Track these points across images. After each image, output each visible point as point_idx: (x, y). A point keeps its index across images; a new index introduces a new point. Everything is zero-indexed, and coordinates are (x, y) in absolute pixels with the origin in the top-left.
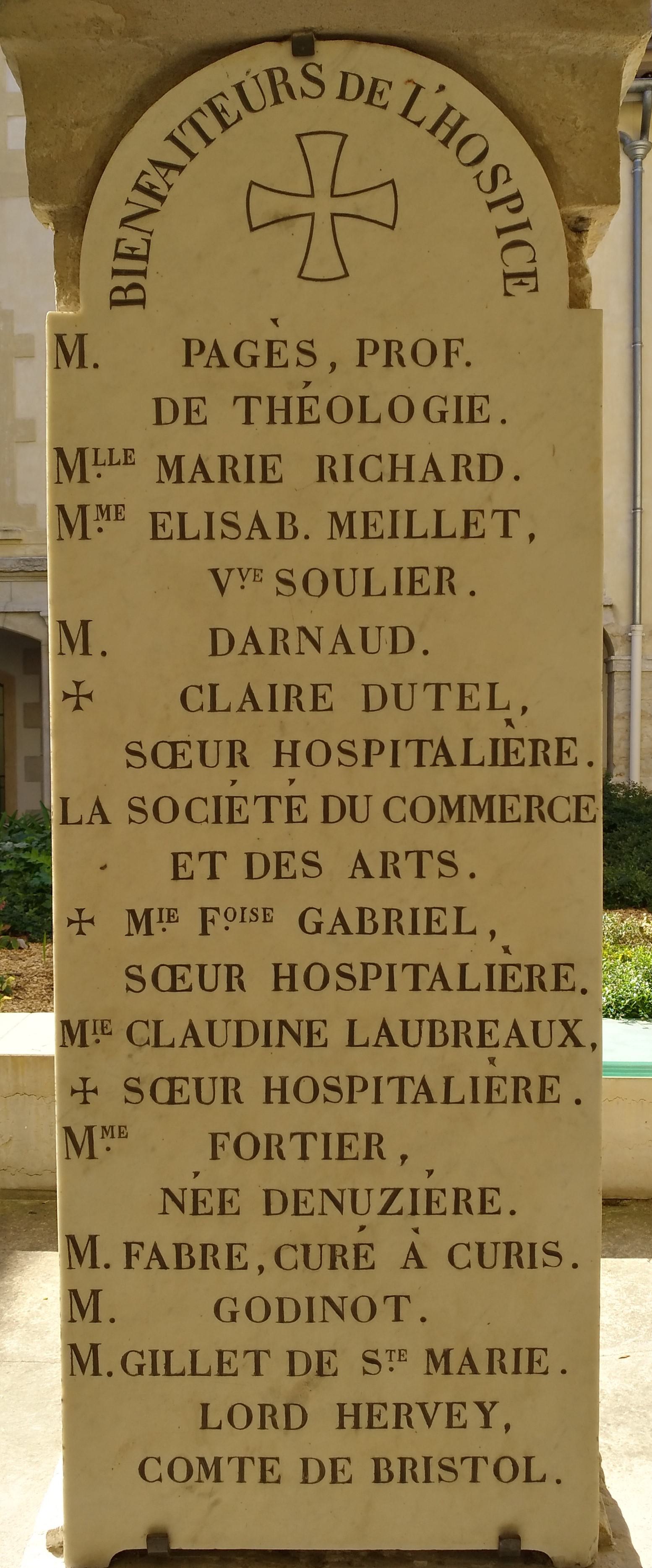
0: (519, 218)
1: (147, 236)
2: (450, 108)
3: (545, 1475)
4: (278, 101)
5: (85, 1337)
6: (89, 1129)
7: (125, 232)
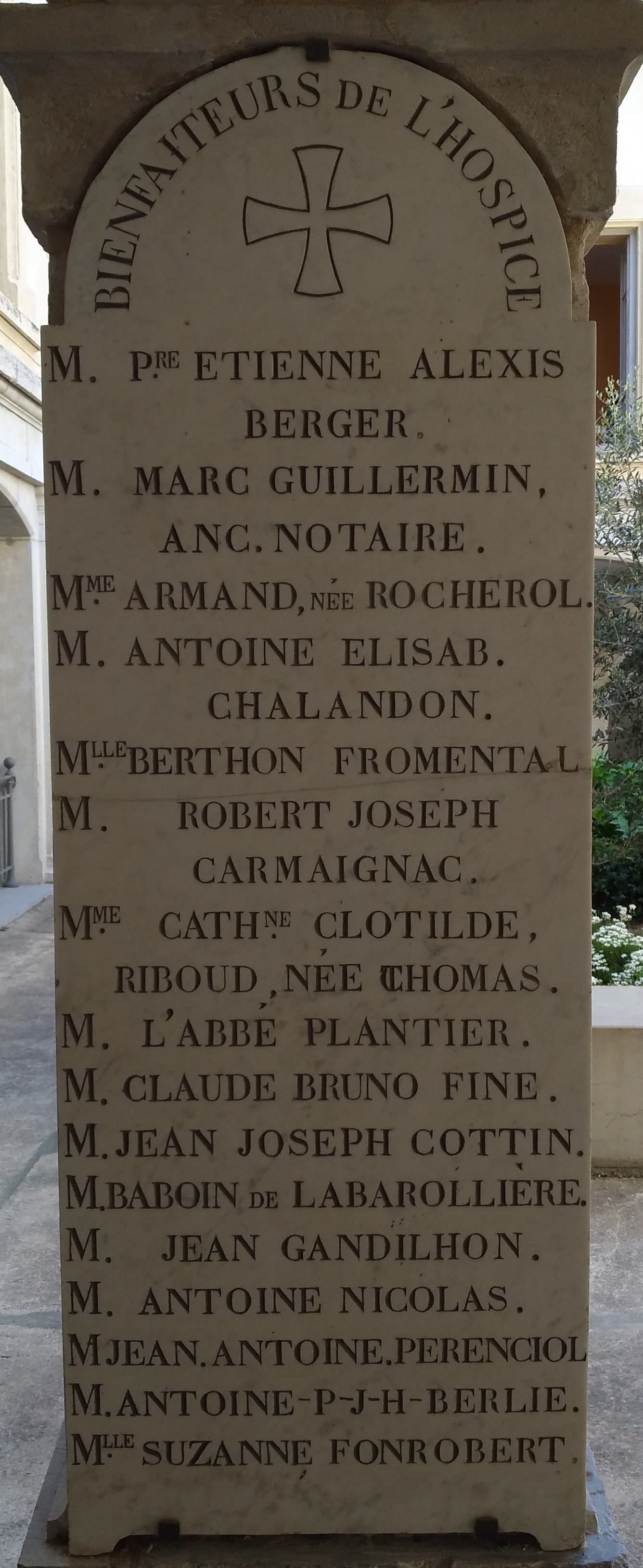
0: (523, 234)
1: (134, 240)
2: (457, 122)
3: (433, 1148)
4: (271, 108)
5: (84, 1276)
6: (78, 579)
7: (111, 233)
